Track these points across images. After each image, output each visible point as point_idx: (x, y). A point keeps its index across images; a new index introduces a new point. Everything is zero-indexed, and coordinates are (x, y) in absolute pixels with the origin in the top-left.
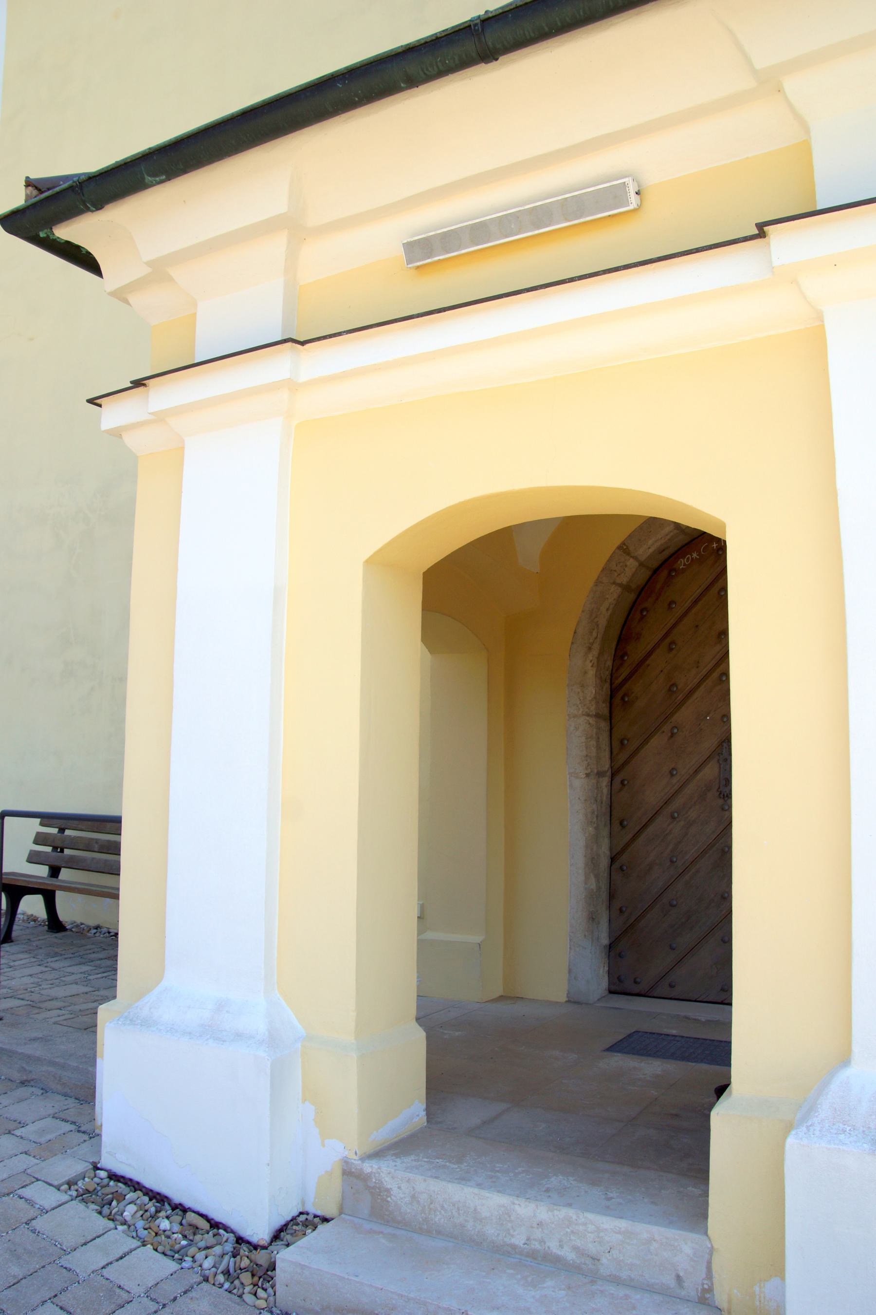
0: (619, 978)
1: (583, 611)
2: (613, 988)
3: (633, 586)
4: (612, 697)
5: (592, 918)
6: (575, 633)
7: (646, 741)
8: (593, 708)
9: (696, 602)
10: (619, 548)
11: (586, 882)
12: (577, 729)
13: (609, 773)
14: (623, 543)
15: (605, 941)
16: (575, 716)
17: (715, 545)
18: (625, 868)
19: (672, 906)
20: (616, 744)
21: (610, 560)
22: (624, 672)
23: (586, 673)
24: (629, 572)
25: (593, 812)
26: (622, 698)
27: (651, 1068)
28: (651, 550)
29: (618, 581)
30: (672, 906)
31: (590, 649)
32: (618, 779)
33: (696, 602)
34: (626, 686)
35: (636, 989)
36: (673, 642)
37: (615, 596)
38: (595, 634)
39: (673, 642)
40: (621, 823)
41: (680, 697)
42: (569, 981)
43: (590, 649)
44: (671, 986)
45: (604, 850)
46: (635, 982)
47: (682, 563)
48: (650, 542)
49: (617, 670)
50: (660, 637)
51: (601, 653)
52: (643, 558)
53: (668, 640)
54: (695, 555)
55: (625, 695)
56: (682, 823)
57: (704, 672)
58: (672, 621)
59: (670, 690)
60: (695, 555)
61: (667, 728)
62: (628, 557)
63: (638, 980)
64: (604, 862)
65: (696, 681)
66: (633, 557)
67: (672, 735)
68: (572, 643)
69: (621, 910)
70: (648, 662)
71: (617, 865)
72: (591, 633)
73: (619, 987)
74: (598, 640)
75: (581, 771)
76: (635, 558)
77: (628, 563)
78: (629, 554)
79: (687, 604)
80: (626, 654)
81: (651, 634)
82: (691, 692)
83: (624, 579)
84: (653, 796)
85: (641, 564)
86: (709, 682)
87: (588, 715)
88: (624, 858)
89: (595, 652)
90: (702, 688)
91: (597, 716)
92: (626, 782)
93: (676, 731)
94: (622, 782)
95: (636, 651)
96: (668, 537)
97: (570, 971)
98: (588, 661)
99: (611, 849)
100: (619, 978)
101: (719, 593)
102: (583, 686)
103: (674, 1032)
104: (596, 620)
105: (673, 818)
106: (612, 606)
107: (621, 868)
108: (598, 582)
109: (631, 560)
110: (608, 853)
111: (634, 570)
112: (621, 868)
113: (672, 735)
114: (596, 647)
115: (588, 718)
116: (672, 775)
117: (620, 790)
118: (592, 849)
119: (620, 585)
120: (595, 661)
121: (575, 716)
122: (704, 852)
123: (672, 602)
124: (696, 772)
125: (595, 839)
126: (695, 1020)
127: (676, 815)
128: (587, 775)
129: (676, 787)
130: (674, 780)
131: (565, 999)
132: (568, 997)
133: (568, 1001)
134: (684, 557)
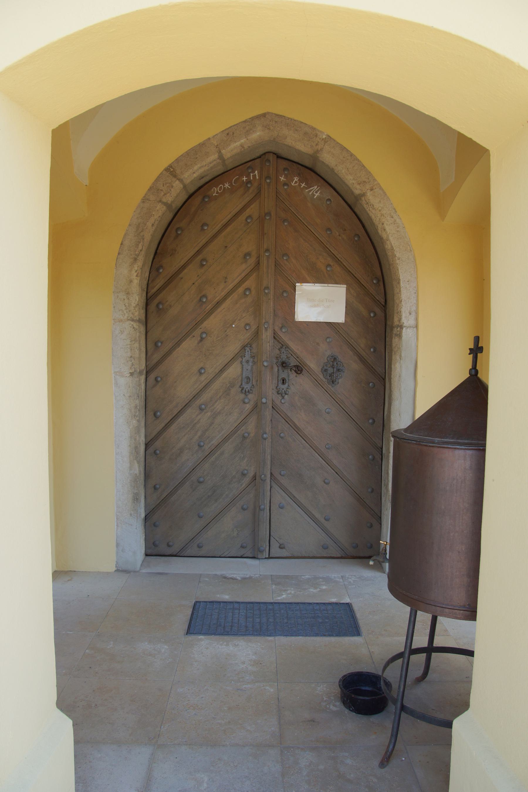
0: (154, 544)
1: (130, 225)
2: (149, 552)
3: (174, 206)
4: (147, 304)
5: (136, 499)
6: (122, 244)
7: (178, 344)
8: (137, 314)
9: (225, 226)
10: (167, 170)
11: (131, 468)
12: (122, 332)
13: (145, 372)
14: (170, 166)
15: (143, 515)
16: (121, 321)
17: (245, 179)
18: (158, 452)
19: (200, 482)
20: (151, 346)
21: (157, 180)
22: (159, 283)
23: (131, 281)
24: (174, 193)
25: (136, 407)
26: (157, 306)
27: (243, 652)
28: (195, 175)
29: (164, 200)
30: (200, 482)
31: (135, 259)
32: (152, 377)
33: (225, 226)
34: (161, 295)
35: (169, 551)
36: (204, 260)
37: (160, 214)
38: (140, 247)
39: (204, 260)
40: (155, 414)
41: (209, 307)
42: (117, 553)
43: (135, 259)
44: (199, 547)
45: (142, 439)
46: (169, 546)
47: (215, 191)
48: (196, 168)
49: (153, 281)
50: (192, 253)
51: (143, 265)
52: (187, 181)
53: (200, 257)
54: (227, 185)
55: (160, 303)
56: (209, 414)
57: (231, 286)
58: (204, 241)
59: (200, 300)
60: (227, 185)
61: (198, 332)
62: (174, 179)
63: (171, 544)
64: (142, 448)
65: (223, 294)
66: (179, 179)
67: (202, 339)
68: (119, 254)
69: (155, 488)
70: (181, 276)
71: (151, 450)
72: (137, 246)
73: (153, 551)
74: (143, 253)
75: (126, 371)
76: (181, 181)
77: (174, 185)
78: (175, 176)
79: (218, 228)
80: (161, 267)
81: (185, 251)
82: (219, 304)
83: (169, 199)
84: (183, 391)
85: (185, 187)
86: (235, 296)
87: (133, 320)
88: (158, 444)
89: (140, 263)
90: (228, 302)
91: (139, 321)
92: (159, 379)
93: (204, 336)
94: (156, 379)
95: (171, 265)
96: (211, 165)
97: (118, 545)
98: (133, 272)
99: (146, 436)
100: (154, 544)
101: (246, 220)
102: (128, 293)
103: (226, 597)
104: (142, 234)
105: (201, 409)
106: (157, 222)
107: (155, 452)
108: (145, 200)
109: (177, 182)
110: (144, 440)
111: (178, 191)
112: (155, 452)
113: (202, 339)
114: (141, 258)
115: (132, 323)
116: (201, 374)
117: (154, 386)
118: (135, 440)
119: (165, 204)
120: (140, 271)
121: (121, 321)
122: (226, 439)
123: (205, 224)
124: (222, 371)
125: (137, 430)
126: (232, 579)
127: (203, 406)
128: (132, 374)
129: (203, 384)
130: (203, 378)
131: (114, 569)
132: (116, 567)
133: (117, 571)
134: (216, 187)
